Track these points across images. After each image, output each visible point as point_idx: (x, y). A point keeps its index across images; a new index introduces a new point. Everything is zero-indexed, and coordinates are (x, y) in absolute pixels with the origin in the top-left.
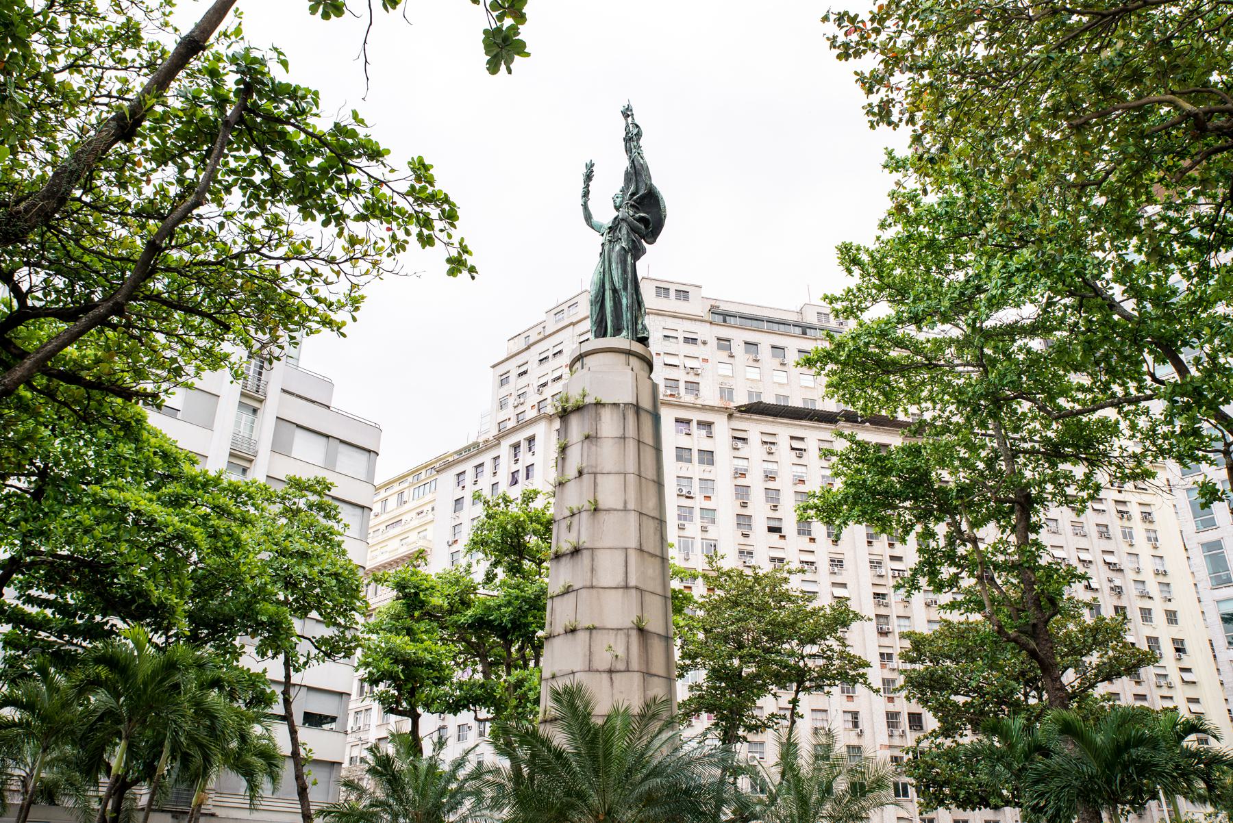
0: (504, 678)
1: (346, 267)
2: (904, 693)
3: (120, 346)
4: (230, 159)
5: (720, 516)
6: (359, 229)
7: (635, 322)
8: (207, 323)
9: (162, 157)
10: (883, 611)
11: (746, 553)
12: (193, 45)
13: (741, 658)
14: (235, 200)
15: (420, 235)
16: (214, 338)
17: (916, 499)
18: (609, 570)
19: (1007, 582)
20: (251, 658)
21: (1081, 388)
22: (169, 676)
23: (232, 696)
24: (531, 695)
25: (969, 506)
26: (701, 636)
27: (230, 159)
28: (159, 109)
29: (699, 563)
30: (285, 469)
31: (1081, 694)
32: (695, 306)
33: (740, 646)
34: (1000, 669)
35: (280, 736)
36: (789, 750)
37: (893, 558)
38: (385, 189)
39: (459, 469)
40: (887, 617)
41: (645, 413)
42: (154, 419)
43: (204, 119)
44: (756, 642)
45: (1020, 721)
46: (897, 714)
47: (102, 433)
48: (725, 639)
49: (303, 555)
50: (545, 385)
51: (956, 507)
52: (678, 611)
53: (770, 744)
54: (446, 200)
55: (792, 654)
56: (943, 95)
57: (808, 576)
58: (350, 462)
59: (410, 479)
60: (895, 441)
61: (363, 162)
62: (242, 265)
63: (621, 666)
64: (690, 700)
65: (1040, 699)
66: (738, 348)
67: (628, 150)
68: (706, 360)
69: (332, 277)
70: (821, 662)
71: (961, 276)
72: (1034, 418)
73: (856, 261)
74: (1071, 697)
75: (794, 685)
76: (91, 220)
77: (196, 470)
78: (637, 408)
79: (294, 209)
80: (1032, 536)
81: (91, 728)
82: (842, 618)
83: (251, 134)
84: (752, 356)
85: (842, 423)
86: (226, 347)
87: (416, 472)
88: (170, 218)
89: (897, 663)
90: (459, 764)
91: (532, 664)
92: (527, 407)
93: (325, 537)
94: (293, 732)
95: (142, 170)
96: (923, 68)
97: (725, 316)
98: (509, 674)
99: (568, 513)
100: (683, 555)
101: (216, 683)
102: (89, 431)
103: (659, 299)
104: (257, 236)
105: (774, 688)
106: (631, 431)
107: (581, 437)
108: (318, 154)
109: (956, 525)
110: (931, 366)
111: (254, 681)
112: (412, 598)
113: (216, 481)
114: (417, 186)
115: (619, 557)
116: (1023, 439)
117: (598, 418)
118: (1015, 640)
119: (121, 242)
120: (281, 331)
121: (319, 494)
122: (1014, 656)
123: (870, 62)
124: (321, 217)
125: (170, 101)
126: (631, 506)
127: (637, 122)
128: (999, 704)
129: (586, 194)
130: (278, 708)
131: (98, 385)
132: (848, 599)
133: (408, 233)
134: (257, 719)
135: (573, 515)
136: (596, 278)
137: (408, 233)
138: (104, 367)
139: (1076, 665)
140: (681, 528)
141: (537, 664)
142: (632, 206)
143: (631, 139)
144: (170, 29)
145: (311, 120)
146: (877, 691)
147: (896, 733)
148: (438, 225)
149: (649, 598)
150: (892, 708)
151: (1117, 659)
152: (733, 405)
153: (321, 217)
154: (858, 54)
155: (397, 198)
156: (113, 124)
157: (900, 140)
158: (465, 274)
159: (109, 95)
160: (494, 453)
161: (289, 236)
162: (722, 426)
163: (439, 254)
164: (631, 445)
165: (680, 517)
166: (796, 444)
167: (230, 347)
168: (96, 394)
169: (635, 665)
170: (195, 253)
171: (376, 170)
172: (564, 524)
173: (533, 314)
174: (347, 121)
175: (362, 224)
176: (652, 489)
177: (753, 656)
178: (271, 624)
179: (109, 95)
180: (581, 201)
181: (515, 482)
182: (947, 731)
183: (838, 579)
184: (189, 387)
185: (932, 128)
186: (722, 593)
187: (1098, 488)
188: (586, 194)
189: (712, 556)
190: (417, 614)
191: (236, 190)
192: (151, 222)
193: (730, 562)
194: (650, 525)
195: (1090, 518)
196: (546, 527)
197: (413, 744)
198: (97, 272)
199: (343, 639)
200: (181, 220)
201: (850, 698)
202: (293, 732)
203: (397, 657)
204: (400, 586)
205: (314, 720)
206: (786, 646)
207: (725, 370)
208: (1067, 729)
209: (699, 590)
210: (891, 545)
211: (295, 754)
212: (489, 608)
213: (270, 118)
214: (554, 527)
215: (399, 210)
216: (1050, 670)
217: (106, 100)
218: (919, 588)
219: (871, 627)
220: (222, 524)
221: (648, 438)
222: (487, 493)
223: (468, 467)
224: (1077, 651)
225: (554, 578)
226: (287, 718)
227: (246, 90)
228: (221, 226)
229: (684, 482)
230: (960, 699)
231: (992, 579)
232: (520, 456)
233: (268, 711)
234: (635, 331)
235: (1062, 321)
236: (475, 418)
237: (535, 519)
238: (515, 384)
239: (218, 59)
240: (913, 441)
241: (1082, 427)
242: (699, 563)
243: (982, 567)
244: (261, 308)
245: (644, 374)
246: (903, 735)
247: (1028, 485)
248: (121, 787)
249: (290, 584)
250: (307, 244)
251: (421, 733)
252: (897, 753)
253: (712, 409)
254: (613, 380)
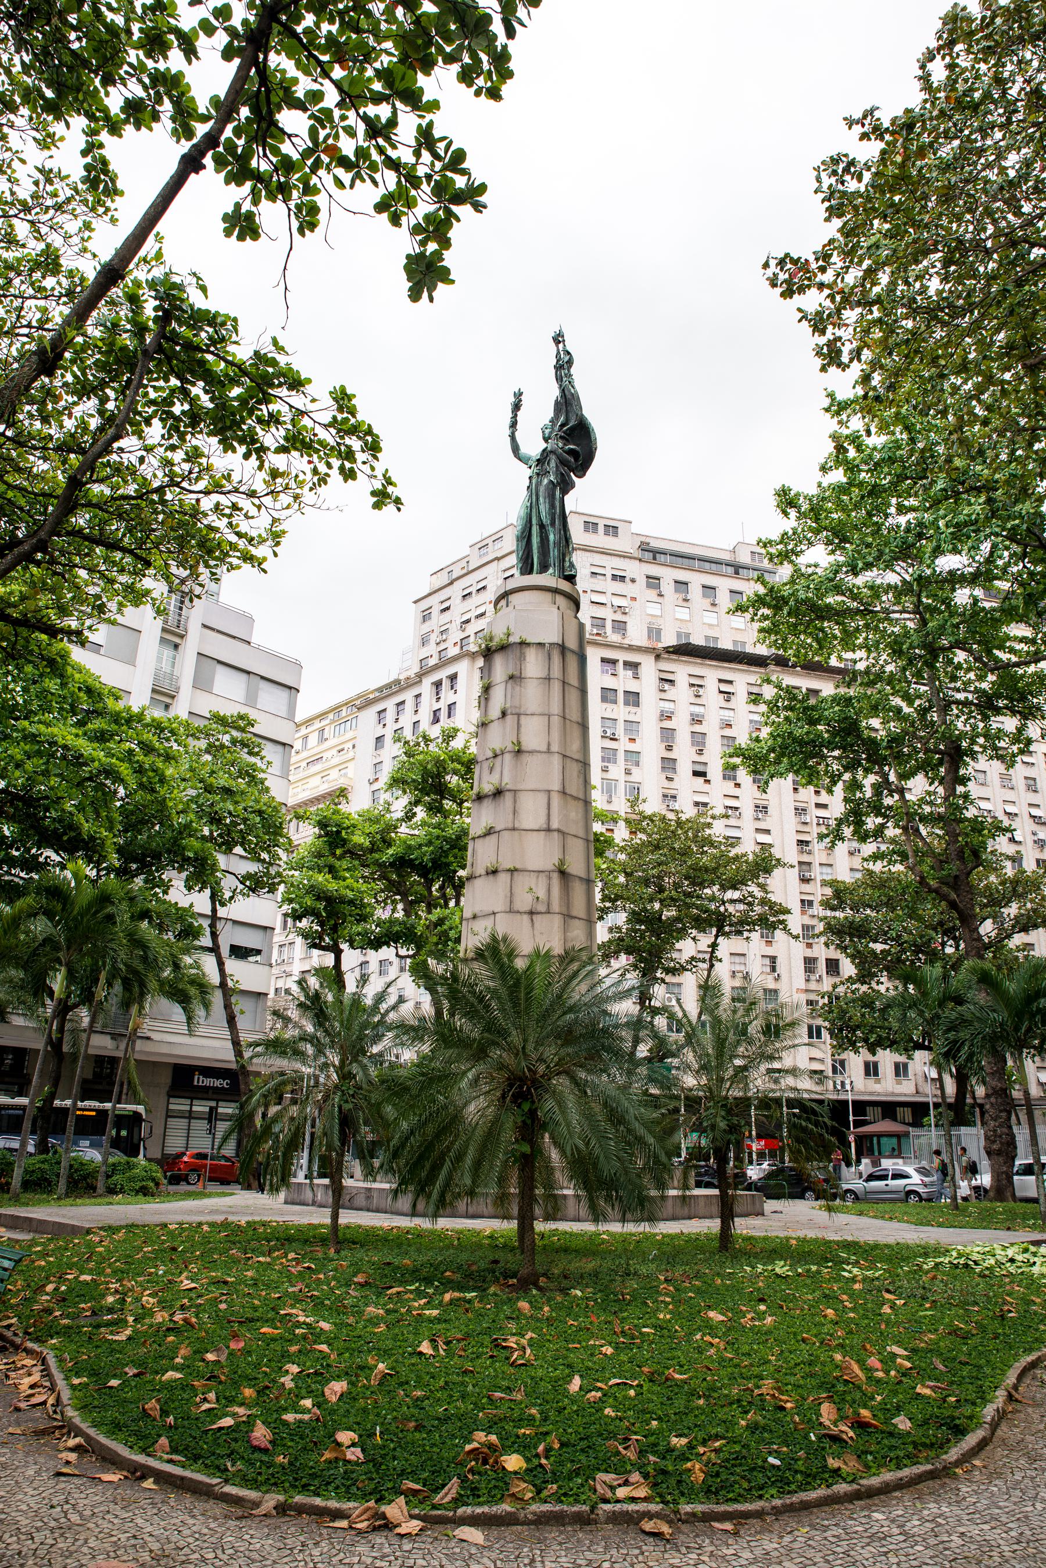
0: (424, 916)
1: (268, 501)
2: (823, 939)
3: (44, 583)
4: (150, 390)
5: (644, 759)
6: (279, 461)
7: (563, 560)
8: (128, 559)
9: (83, 390)
10: (805, 858)
11: (669, 797)
12: (112, 273)
13: (661, 901)
14: (155, 431)
15: (342, 469)
16: (135, 573)
17: (844, 748)
18: (532, 812)
19: (931, 834)
20: (180, 893)
21: (1023, 640)
22: (102, 908)
23: (161, 928)
24: (452, 934)
25: (899, 757)
26: (622, 879)
27: (150, 390)
28: (80, 339)
29: (621, 806)
30: (206, 705)
31: (998, 944)
32: (624, 543)
33: (661, 890)
34: (920, 919)
35: (209, 965)
36: (708, 990)
37: (818, 806)
38: (306, 421)
39: (380, 707)
40: (809, 864)
41: (571, 654)
42: (77, 654)
43: (124, 348)
44: (677, 886)
45: (937, 970)
46: (815, 959)
47: (29, 669)
48: (646, 882)
49: (227, 791)
50: (468, 621)
51: (885, 758)
52: (600, 853)
53: (689, 984)
54: (369, 432)
55: (712, 899)
56: (893, 332)
57: (732, 822)
58: (270, 699)
59: (331, 716)
60: (827, 688)
61: (283, 392)
62: (163, 502)
63: (541, 908)
64: (610, 941)
65: (957, 948)
66: (667, 587)
67: (559, 379)
68: (634, 599)
69: (253, 512)
70: (741, 907)
71: (902, 520)
72: (969, 670)
73: (792, 504)
74: (987, 947)
75: (714, 930)
76: (14, 454)
77: (120, 706)
78: (563, 648)
79: (214, 440)
80: (960, 789)
81: (35, 953)
82: (764, 864)
83: (169, 363)
84: (682, 596)
85: (772, 667)
86: (147, 583)
87: (336, 709)
88: (91, 453)
89: (818, 910)
90: (380, 997)
91: (452, 903)
92: (449, 644)
93: (250, 775)
94: (221, 964)
95: (63, 403)
96: (872, 304)
97: (656, 553)
98: (429, 912)
99: (490, 754)
100: (606, 797)
101: (145, 914)
102: (17, 667)
104: (176, 469)
105: (694, 932)
106: (556, 672)
107: (505, 677)
108: (239, 384)
109: (885, 776)
110: (866, 612)
111: (183, 915)
112: (334, 836)
113: (140, 717)
114: (339, 417)
115: (542, 799)
116: (958, 690)
117: (522, 658)
118: (936, 891)
119: (42, 477)
120: (201, 569)
121: (243, 730)
122: (934, 906)
123: (813, 300)
124: (242, 450)
125: (90, 330)
126: (555, 748)
128: (916, 952)
129: (514, 425)
130: (206, 941)
131: (24, 622)
132: (771, 845)
133: (329, 466)
134: (187, 951)
135: (496, 756)
136: (523, 513)
137: (329, 466)
138: (30, 605)
139: (996, 917)
140: (605, 770)
141: (457, 903)
143: (561, 367)
144: (88, 255)
145: (231, 348)
146: (796, 937)
147: (813, 978)
148: (360, 457)
149: (570, 841)
150: (809, 953)
151: (1034, 911)
152: (660, 645)
153: (242, 450)
154: (802, 290)
155: (319, 430)
156: (34, 358)
157: (845, 383)
158: (391, 508)
159: (29, 326)
160: (415, 691)
161: (208, 469)
162: (649, 667)
163: (363, 486)
164: (556, 686)
165: (603, 759)
166: (725, 687)
167: (153, 584)
168: (24, 632)
169: (556, 906)
170: (114, 488)
171: (298, 401)
172: (486, 765)
173: (455, 548)
174: (268, 349)
175: (283, 457)
176: (576, 732)
177: (672, 899)
178: (196, 859)
179: (29, 326)
180: (508, 432)
181: (436, 720)
182: (864, 976)
183: (762, 825)
184: (113, 623)
185: (882, 367)
186: (644, 837)
187: (1029, 742)
188: (514, 425)
189: (634, 802)
190: (338, 852)
191: (156, 422)
192: (72, 456)
193: (652, 805)
194: (574, 769)
195: (1019, 771)
196: (468, 766)
197: (335, 977)
198: (21, 509)
199: (267, 874)
200: (100, 455)
201: (769, 943)
202: (221, 964)
203: (321, 895)
204: (322, 824)
205: (240, 952)
206: (707, 891)
207: (654, 609)
208: (985, 979)
209: (621, 834)
210: (817, 793)
211: (223, 985)
212: (410, 847)
213: (191, 347)
214: (477, 770)
215: (321, 442)
216: (969, 921)
217: (25, 331)
218: (842, 839)
219: (793, 874)
220: (147, 761)
221: (573, 679)
222: (408, 734)
223: (390, 704)
224: (996, 902)
225: (476, 819)
226: (215, 950)
227: (165, 317)
228: (142, 460)
229: (609, 723)
230: (878, 947)
231: (917, 830)
232: (442, 695)
233: (197, 943)
234: (562, 569)
235: (1004, 570)
236: (396, 659)
237: (455, 758)
238: (437, 620)
239: (137, 284)
240: (842, 691)
241: (1016, 679)
242: (621, 806)
243: (909, 818)
244: (182, 543)
245: (570, 613)
246: (820, 980)
247: (959, 738)
248: (64, 1009)
249: (215, 820)
250: (228, 477)
251: (344, 967)
252: (813, 997)
253: (639, 649)
254: (539, 619)
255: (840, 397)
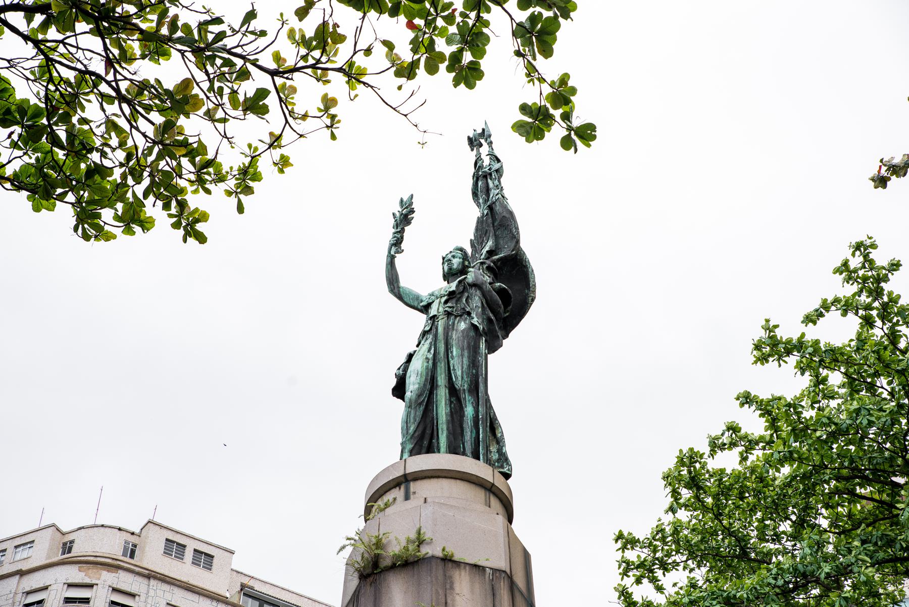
103: (167, 560)
127: (497, 153)
129: (397, 243)
142: (489, 268)
188: (397, 243)
255: (783, 334)
